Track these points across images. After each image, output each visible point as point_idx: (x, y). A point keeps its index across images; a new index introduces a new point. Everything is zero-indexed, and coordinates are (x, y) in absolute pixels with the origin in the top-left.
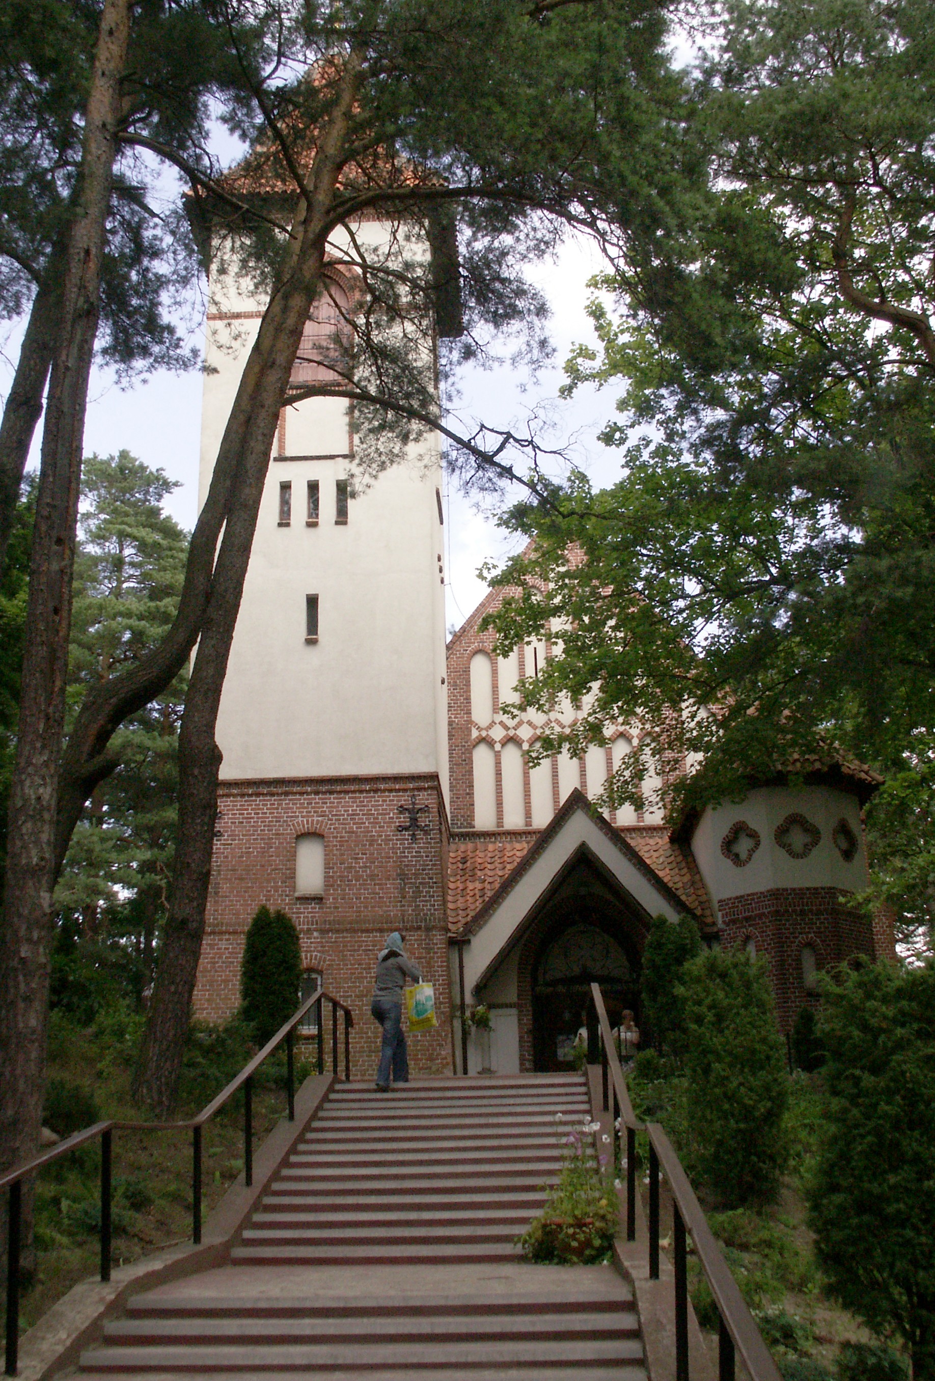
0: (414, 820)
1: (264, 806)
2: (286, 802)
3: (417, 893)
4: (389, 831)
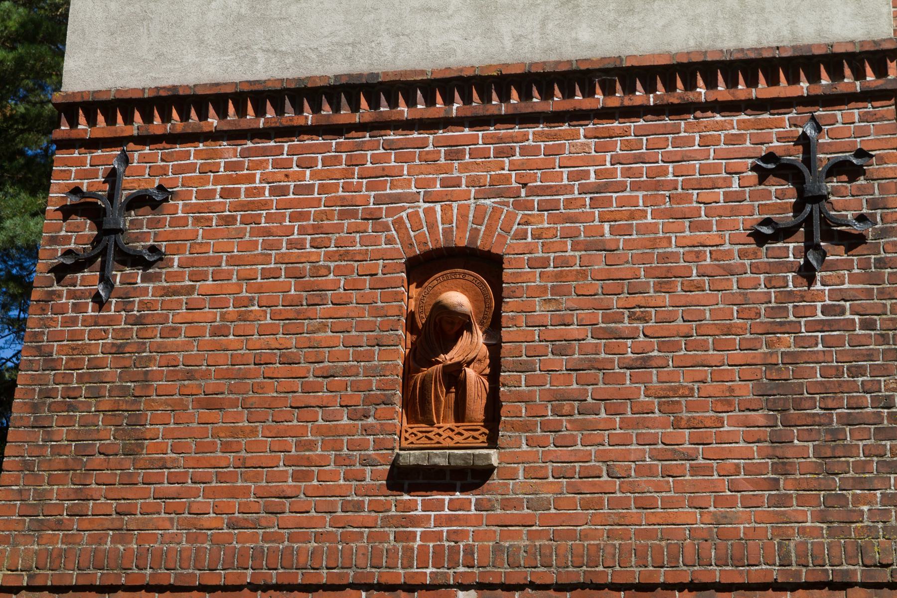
0: (807, 199)
1: (310, 169)
2: (372, 150)
3: (827, 464)
4: (729, 238)
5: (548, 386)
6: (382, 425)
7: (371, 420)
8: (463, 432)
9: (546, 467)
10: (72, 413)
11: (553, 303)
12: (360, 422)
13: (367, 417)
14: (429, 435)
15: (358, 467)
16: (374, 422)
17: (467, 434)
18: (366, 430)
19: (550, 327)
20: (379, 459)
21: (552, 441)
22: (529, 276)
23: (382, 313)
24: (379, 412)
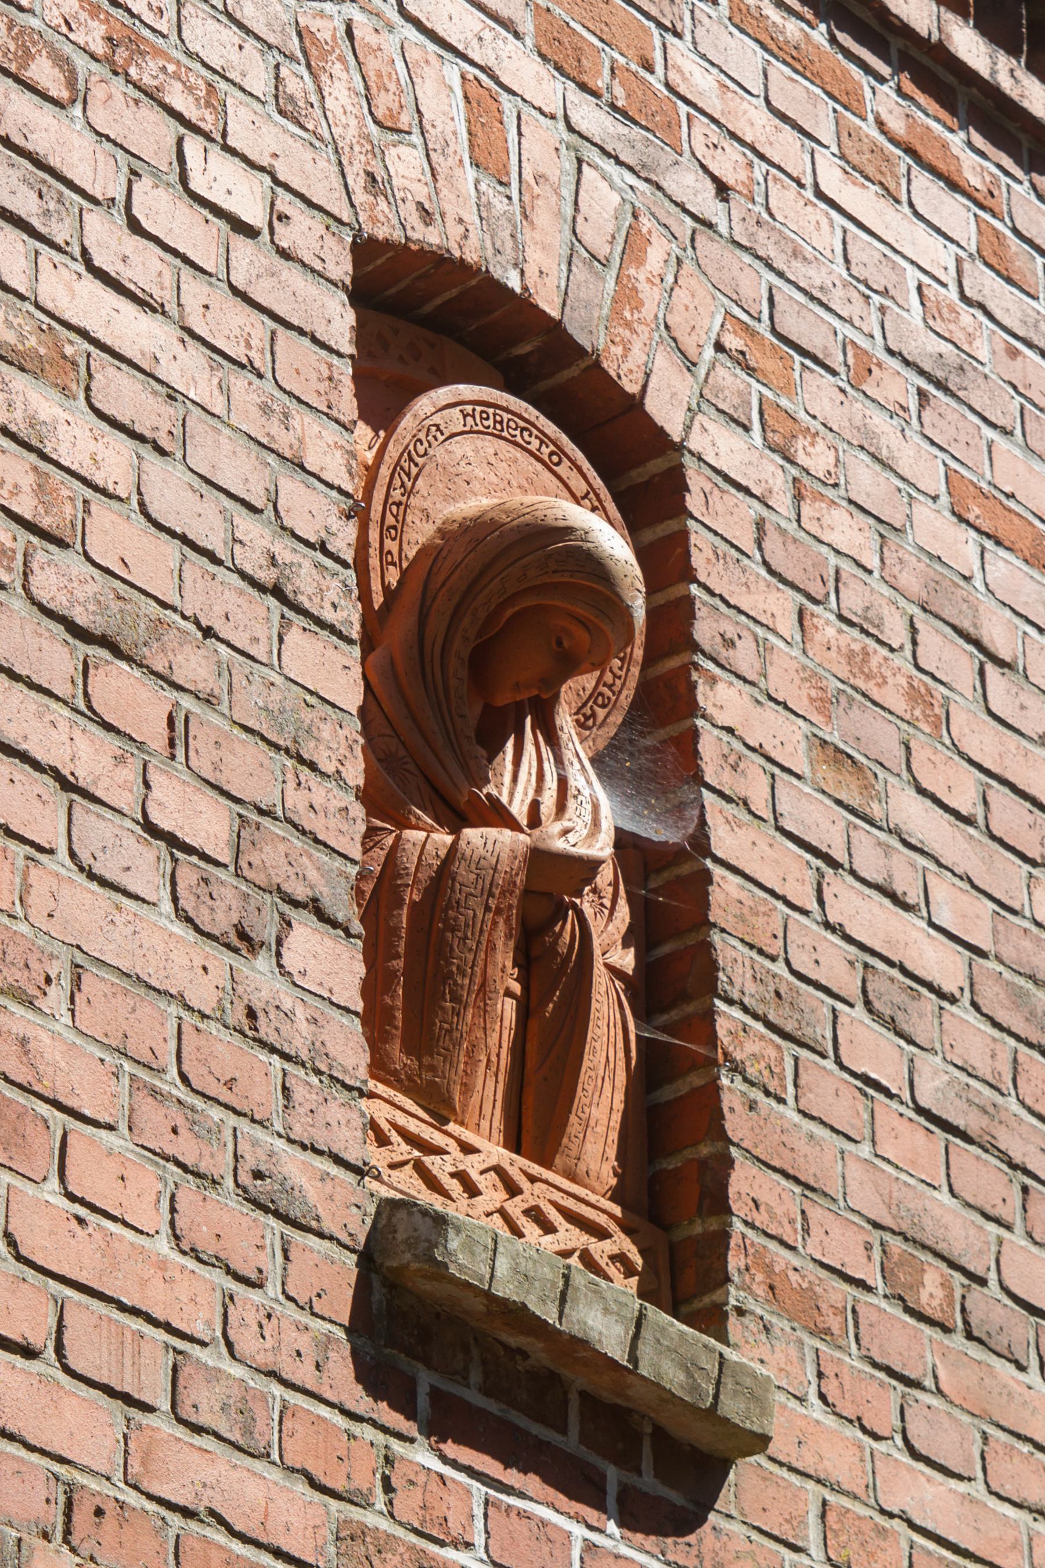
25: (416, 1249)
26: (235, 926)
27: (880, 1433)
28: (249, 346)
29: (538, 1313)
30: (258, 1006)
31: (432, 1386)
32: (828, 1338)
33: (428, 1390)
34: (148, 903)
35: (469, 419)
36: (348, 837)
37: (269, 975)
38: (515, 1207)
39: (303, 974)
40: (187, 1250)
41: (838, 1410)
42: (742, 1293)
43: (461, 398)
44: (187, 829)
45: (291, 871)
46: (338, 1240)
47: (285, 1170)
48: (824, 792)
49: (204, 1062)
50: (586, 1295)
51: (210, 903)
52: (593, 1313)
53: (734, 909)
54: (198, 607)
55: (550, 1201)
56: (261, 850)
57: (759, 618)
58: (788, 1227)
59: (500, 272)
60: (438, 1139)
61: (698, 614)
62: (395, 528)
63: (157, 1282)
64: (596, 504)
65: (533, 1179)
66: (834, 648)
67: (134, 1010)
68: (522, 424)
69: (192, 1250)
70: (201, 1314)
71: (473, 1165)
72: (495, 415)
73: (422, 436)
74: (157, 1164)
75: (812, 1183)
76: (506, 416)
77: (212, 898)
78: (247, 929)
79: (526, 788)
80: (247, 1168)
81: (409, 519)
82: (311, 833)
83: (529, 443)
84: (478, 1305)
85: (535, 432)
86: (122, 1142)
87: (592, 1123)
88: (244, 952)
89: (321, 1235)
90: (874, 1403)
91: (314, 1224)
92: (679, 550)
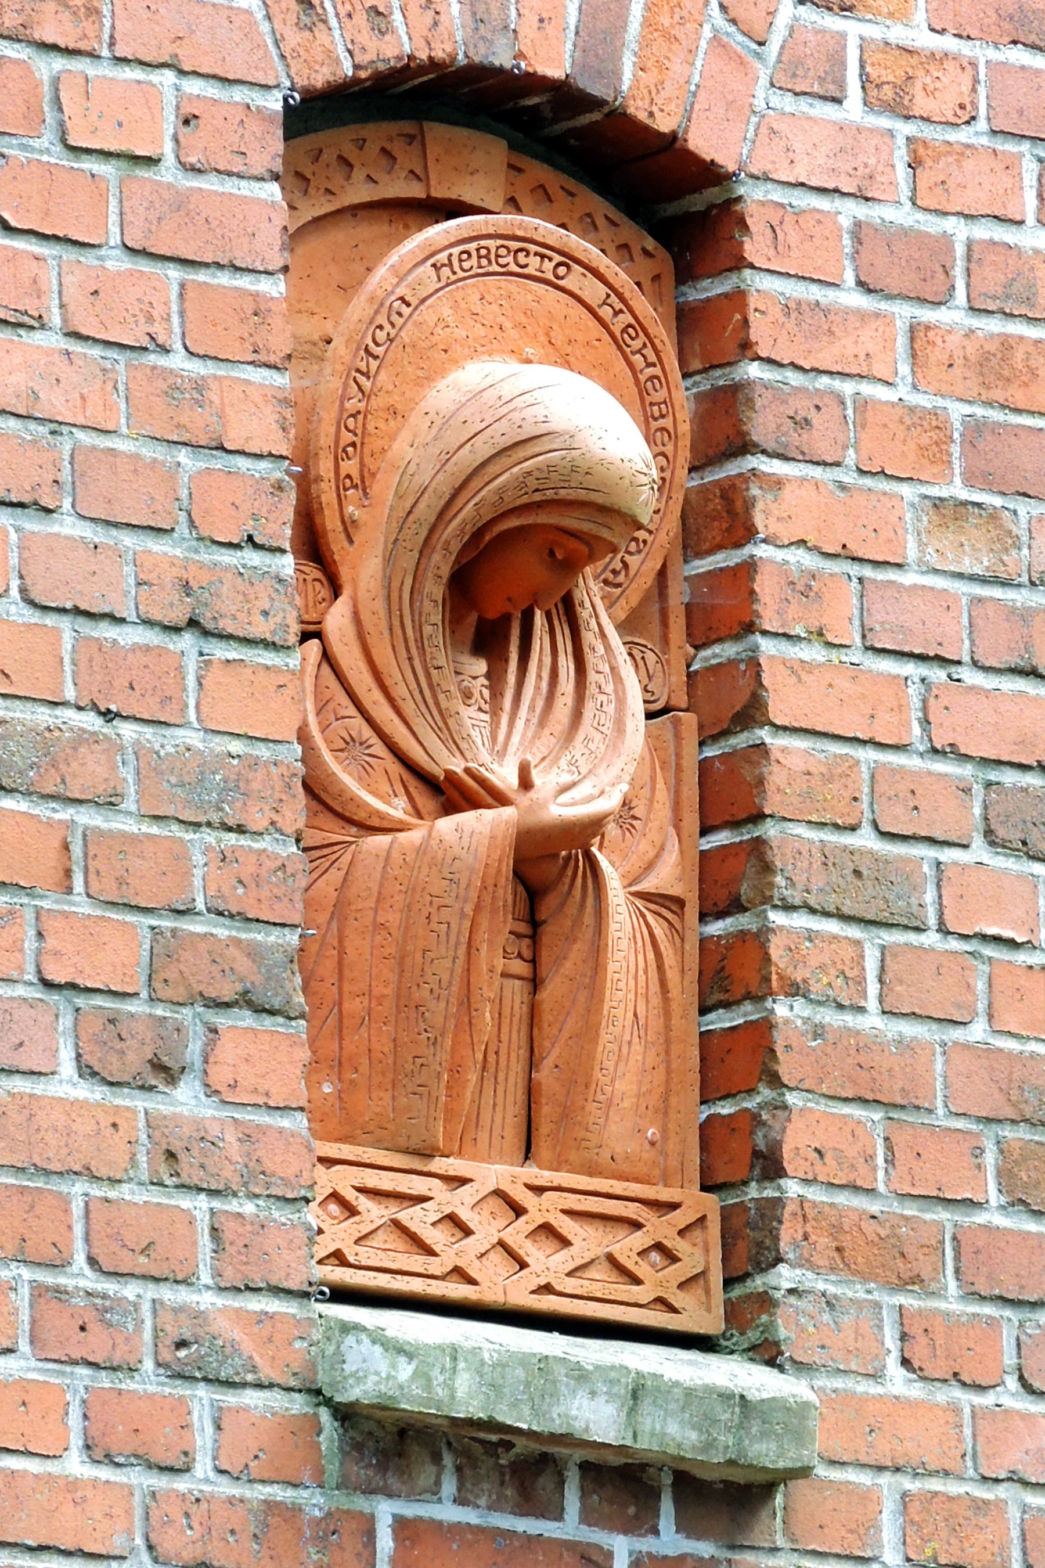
5: (978, 1031)
6: (248, 1136)
7: (186, 1099)
8: (567, 1226)
9: (1000, 1505)
10: (725, 1109)
11: (974, 531)
12: (140, 1102)
13: (167, 1072)
14: (413, 1217)
15: (149, 1381)
16: (208, 1110)
17: (588, 1241)
18: (172, 1160)
19: (970, 676)
20: (247, 1347)
21: (1009, 1359)
22: (868, 339)
23: (199, 422)
24: (227, 1050)
25: (365, 1384)
26: (150, 1061)
27: (983, 1384)
28: (150, 319)
29: (509, 1422)
30: (177, 1147)
31: (394, 1516)
32: (916, 1288)
33: (390, 1521)
34: (46, 1074)
35: (446, 271)
36: (286, 900)
37: (193, 1102)
38: (517, 1234)
39: (233, 1086)
40: (101, 1459)
41: (926, 1373)
42: (798, 1272)
43: (433, 248)
44: (88, 970)
45: (215, 969)
46: (279, 1386)
47: (214, 1329)
48: (936, 571)
49: (117, 1237)
50: (567, 1385)
51: (119, 1045)
52: (577, 1402)
53: (800, 785)
54: (95, 689)
55: (565, 1212)
56: (178, 960)
57: (847, 371)
58: (863, 1168)
59: (482, 51)
60: (417, 1185)
61: (759, 403)
62: (353, 444)
63: (68, 1508)
64: (621, 306)
65: (539, 1190)
66: (959, 362)
67: (32, 1207)
68: (515, 245)
69: (107, 1456)
70: (117, 1528)
71: (461, 1202)
72: (478, 250)
73: (382, 320)
74: (63, 1373)
75: (899, 1100)
76: (492, 244)
77: (121, 1039)
78: (165, 1059)
79: (533, 700)
80: (168, 1342)
81: (370, 427)
82: (239, 914)
83: (526, 266)
84: (445, 1422)
85: (533, 248)
86: (23, 1363)
87: (616, 1101)
88: (161, 1088)
89: (259, 1386)
90: (978, 1349)
91: (250, 1377)
92: (738, 316)
